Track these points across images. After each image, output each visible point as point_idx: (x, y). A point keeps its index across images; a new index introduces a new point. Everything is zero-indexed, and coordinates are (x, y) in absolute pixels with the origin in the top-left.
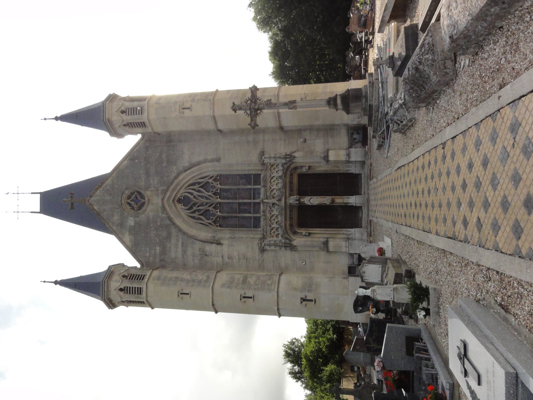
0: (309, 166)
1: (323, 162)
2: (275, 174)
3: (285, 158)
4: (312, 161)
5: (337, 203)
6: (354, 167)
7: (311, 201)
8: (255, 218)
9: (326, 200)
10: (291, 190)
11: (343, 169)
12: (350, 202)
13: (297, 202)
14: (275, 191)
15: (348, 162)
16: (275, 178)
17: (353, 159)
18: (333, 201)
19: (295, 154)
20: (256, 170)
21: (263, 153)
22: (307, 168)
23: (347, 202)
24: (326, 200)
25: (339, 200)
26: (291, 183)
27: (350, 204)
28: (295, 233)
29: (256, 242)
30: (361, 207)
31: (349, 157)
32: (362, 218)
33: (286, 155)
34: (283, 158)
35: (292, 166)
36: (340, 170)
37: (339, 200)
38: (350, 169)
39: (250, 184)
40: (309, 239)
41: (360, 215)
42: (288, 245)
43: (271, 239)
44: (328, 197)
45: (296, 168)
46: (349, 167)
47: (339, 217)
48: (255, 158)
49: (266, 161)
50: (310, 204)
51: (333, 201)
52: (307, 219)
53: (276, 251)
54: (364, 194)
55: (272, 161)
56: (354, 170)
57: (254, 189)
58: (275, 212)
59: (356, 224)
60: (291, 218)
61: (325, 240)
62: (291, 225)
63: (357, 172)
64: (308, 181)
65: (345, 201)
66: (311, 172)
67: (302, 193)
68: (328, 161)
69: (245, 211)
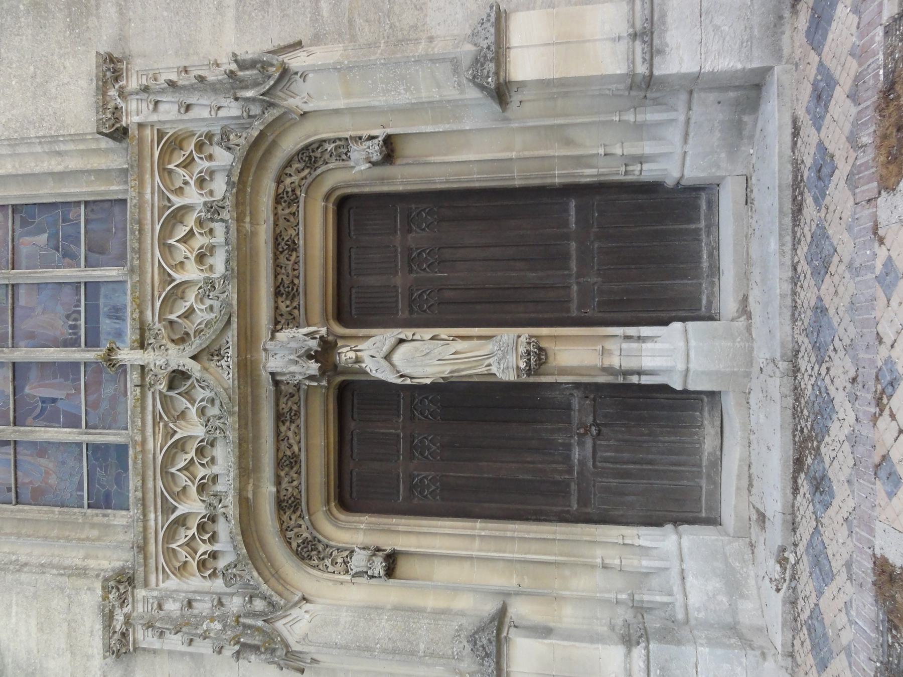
0: (388, 141)
1: (479, 111)
2: (193, 197)
3: (233, 83)
4: (403, 98)
5: (563, 371)
6: (674, 135)
7: (397, 357)
8: (96, 450)
9: (491, 353)
10: (285, 291)
11: (603, 151)
12: (647, 363)
13: (313, 367)
14: (191, 297)
15: (646, 88)
16: (191, 221)
17: (680, 59)
18: (538, 357)
19: (297, 61)
20: (99, 173)
21: (112, 69)
22: (375, 151)
23: (629, 364)
24: (491, 353)
25: (581, 354)
26: (284, 246)
27: (645, 380)
28: (309, 551)
29: (91, 597)
30: (714, 395)
31: (653, 53)
32: (716, 463)
33: (243, 65)
34: (214, 88)
35: (291, 143)
36: (579, 160)
37: (581, 354)
38: (648, 148)
39: (70, 257)
40: (389, 593)
41: (709, 445)
42: (257, 640)
43: (173, 583)
44: (507, 334)
45: (310, 156)
46: (640, 130)
47: (576, 454)
48: (75, 102)
49: (135, 113)
50: (393, 379)
51: (538, 357)
52: (396, 458)
53: (196, 658)
54: (744, 310)
55: (169, 111)
56: (670, 154)
57: (92, 288)
58: (194, 428)
59: (679, 503)
60: (287, 462)
61: (490, 607)
62: (286, 505)
63: (694, 172)
64: (401, 240)
65: (615, 361)
66: (401, 178)
67: (355, 306)
68: (501, 93)
69: (49, 413)
